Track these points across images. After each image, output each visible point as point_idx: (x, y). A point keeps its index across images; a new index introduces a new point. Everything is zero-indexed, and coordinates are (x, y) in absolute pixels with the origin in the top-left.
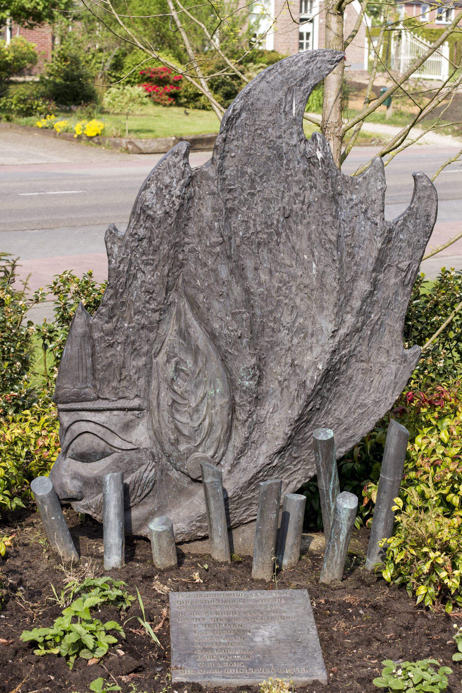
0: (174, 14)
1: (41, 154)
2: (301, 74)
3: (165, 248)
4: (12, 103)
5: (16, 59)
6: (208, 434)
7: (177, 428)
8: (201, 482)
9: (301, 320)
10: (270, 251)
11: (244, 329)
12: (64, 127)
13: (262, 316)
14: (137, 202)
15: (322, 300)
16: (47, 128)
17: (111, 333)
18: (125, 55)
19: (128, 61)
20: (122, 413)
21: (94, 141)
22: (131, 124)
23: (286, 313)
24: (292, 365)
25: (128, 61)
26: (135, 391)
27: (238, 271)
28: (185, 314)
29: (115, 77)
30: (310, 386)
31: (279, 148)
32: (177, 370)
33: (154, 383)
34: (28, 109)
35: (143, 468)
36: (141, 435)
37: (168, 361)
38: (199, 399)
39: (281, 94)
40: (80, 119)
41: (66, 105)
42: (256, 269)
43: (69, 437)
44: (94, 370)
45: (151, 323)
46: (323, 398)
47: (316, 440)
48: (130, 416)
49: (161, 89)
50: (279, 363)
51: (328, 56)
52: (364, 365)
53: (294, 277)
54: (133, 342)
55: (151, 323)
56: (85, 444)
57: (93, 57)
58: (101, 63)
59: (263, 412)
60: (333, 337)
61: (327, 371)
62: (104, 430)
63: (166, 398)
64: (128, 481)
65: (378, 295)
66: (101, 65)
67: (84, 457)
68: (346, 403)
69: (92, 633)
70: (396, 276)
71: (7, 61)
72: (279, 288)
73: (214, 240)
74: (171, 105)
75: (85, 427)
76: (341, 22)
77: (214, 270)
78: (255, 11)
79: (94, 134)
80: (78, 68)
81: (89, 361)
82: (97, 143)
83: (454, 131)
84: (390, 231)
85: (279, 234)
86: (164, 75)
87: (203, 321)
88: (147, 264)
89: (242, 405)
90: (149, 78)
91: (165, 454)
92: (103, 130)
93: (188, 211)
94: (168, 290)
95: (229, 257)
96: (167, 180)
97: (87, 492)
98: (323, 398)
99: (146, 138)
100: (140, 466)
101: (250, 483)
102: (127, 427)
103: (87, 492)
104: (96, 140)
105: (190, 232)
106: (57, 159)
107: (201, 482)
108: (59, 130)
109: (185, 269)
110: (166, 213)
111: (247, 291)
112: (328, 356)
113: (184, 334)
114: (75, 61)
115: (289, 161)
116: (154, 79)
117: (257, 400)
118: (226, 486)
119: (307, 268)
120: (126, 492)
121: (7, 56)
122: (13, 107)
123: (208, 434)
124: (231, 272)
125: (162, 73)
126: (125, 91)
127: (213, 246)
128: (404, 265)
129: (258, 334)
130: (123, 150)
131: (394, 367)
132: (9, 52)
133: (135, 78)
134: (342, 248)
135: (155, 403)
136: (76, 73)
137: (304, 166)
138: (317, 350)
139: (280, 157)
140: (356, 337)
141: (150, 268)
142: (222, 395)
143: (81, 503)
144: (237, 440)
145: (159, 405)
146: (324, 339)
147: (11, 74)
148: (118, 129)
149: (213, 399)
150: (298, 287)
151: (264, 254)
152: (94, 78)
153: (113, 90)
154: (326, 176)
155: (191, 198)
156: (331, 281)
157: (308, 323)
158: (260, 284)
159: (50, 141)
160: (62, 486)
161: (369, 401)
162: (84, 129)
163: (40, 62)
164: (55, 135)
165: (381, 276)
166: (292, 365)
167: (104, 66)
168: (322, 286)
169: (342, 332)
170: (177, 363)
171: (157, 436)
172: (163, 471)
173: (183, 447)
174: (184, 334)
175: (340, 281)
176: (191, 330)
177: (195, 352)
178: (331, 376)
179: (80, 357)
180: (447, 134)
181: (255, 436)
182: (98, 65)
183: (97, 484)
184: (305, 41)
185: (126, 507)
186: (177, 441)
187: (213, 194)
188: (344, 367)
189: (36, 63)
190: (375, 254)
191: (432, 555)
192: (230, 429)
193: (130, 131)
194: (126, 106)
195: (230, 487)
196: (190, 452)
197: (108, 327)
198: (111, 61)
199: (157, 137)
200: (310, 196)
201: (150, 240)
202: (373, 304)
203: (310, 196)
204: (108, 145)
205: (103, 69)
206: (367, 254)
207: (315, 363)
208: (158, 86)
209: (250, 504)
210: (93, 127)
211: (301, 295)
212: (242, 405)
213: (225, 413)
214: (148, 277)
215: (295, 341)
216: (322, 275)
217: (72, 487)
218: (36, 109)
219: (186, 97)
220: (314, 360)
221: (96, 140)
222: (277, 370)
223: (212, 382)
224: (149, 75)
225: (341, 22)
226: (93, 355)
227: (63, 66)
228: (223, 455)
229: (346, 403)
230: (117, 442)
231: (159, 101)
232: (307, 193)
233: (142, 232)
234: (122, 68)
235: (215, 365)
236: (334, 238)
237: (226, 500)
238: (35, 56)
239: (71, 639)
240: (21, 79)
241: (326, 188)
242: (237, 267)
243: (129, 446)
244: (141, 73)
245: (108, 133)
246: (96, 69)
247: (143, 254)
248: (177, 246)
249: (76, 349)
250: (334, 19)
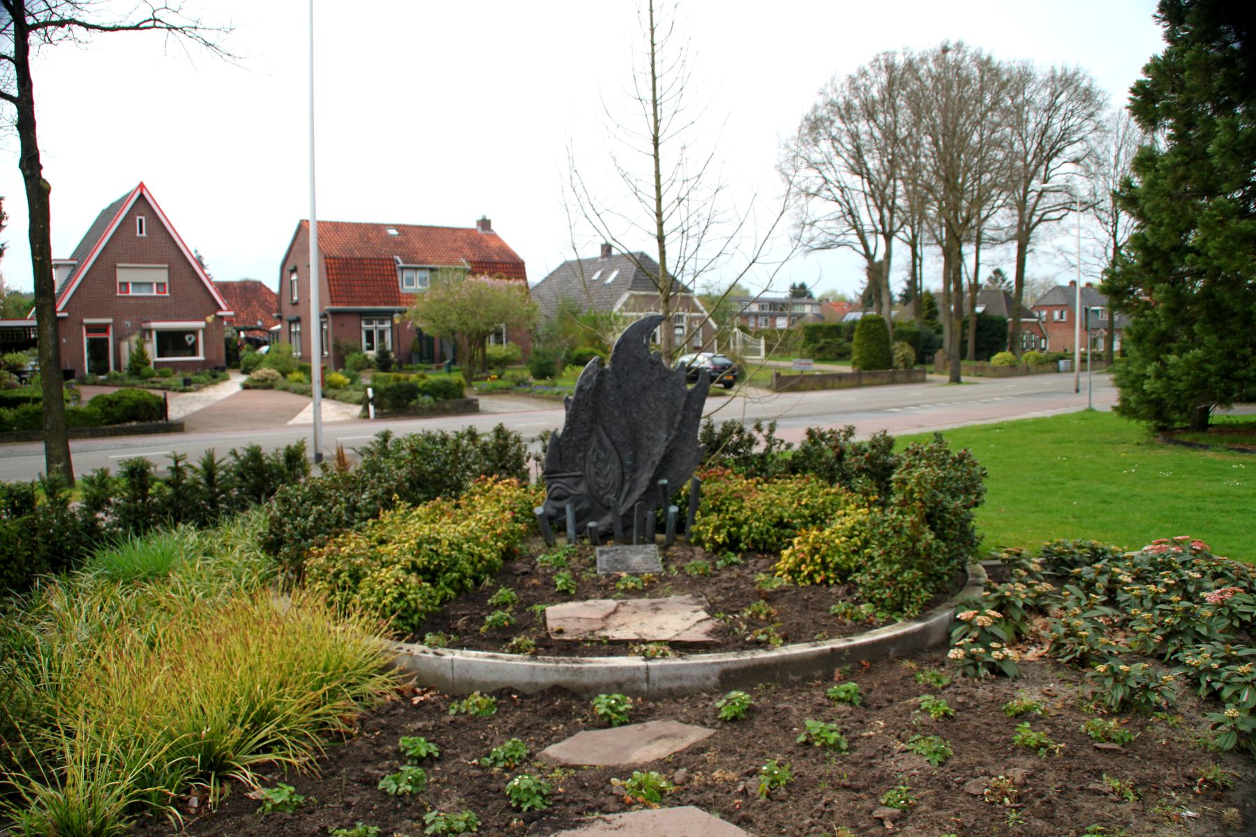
28: (248, 714)
36: (582, 488)
63: (593, 470)
87: (608, 436)
89: (628, 472)
102: (576, 484)
113: (600, 441)
117: (635, 470)
171: (589, 488)
174: (600, 441)
177: (605, 450)
220: (659, 450)
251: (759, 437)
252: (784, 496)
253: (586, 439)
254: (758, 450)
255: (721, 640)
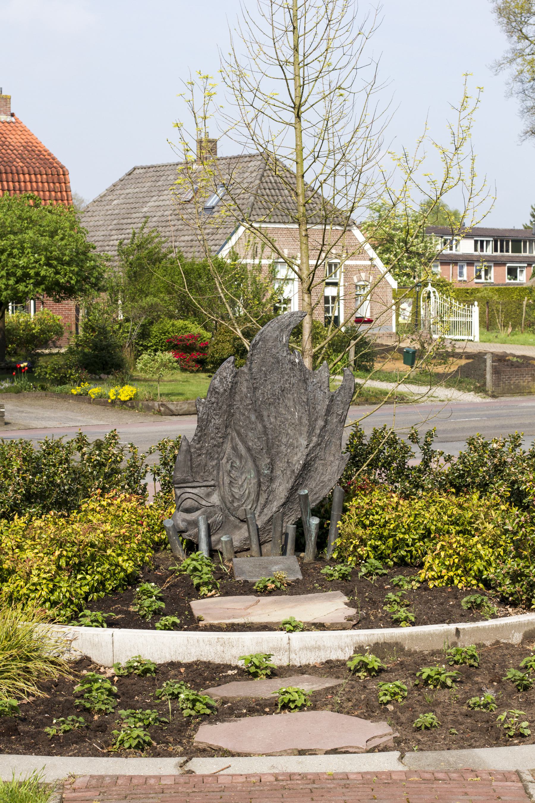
0: (222, 295)
1: (79, 418)
2: (287, 323)
3: (224, 407)
4: (46, 373)
5: (42, 331)
6: (248, 498)
7: (232, 495)
8: (245, 521)
9: (291, 440)
10: (275, 407)
11: (264, 445)
12: (98, 393)
13: (272, 439)
14: (210, 385)
15: (301, 430)
16: (81, 395)
17: (200, 449)
18: (151, 323)
19: (155, 329)
20: (205, 488)
21: (128, 406)
22: (161, 389)
23: (284, 437)
24: (288, 462)
25: (155, 329)
26: (212, 477)
27: (260, 417)
29: (142, 345)
30: (297, 472)
31: (278, 358)
32: (232, 466)
33: (221, 473)
34: (62, 377)
35: (217, 515)
36: (215, 499)
37: (227, 462)
38: (243, 480)
39: (277, 332)
40: (113, 386)
41: (96, 374)
42: (269, 416)
43: (180, 501)
44: (192, 467)
45: (219, 443)
46: (303, 478)
47: (299, 495)
48: (210, 489)
49: (188, 356)
50: (281, 462)
51: (299, 314)
52: (323, 462)
53: (287, 420)
54: (210, 453)
55: (219, 443)
56: (188, 504)
57: (120, 328)
58: (128, 332)
59: (274, 486)
60: (307, 448)
61: (305, 465)
62: (197, 497)
63: (227, 480)
64: (209, 522)
65: (328, 427)
66: (129, 334)
67: (188, 511)
68: (315, 481)
69: (200, 564)
70: (336, 418)
71: (34, 334)
72: (280, 425)
73: (248, 402)
74: (198, 371)
75: (188, 495)
76: (310, 297)
77: (248, 417)
78: (279, 276)
79: (127, 398)
80: (105, 338)
81: (189, 463)
82: (130, 407)
83: (476, 387)
84: (333, 396)
85: (279, 399)
86: (190, 342)
88: (216, 415)
89: (264, 483)
90: (176, 345)
91: (227, 508)
92: (136, 395)
93: (235, 389)
94: (226, 427)
95: (255, 410)
96: (225, 374)
97: (190, 528)
98: (303, 478)
99: (177, 400)
100: (215, 514)
101: (269, 521)
102: (209, 495)
103: (190, 528)
104: (130, 405)
105: (236, 399)
106: (95, 422)
107: (245, 521)
108: (93, 396)
109: (234, 417)
110: (225, 390)
111: (264, 427)
112: (305, 457)
113: (235, 448)
114: (103, 331)
115: (283, 364)
116: (180, 346)
117: (271, 480)
118: (257, 523)
119: (293, 414)
120: (209, 528)
121: (34, 329)
122: (48, 376)
123: (248, 498)
124: (257, 418)
125: (188, 340)
126: (156, 357)
127: (248, 405)
128: (340, 412)
129: (271, 448)
130: (156, 412)
131: (337, 462)
132: (35, 325)
133: (162, 346)
134: (310, 405)
135: (221, 483)
136: (104, 343)
137: (290, 366)
138: (300, 454)
139: (278, 362)
140: (318, 448)
141: (217, 417)
142: (254, 478)
143: (187, 534)
144: (262, 500)
145: (223, 483)
146: (302, 449)
147: (37, 347)
148: (150, 393)
149: (250, 480)
150: (289, 425)
151: (272, 409)
152: (122, 346)
153: (145, 356)
154: (301, 371)
155: (236, 383)
156: (305, 421)
157: (295, 442)
158: (271, 424)
159: (85, 406)
160: (178, 525)
161: (326, 480)
162: (117, 394)
163: (66, 334)
164: (90, 401)
165: (329, 418)
166: (288, 462)
167: (131, 335)
168: (301, 423)
169: (311, 445)
170: (232, 463)
171: (223, 499)
172: (226, 517)
173: (235, 504)
174: (235, 448)
175: (309, 421)
176: (238, 447)
177: (240, 457)
178: (307, 467)
179: (185, 461)
180: (469, 391)
181: (271, 498)
182: (125, 335)
183: (195, 524)
184: (331, 305)
185: (209, 536)
186: (233, 501)
187: (247, 380)
188: (313, 463)
189: (62, 334)
190: (325, 407)
191: (354, 542)
192: (258, 495)
193: (161, 395)
194: (157, 371)
195: (259, 524)
196: (239, 507)
197: (197, 446)
198: (137, 330)
199: (187, 399)
200: (293, 380)
201: (217, 403)
202: (326, 431)
203: (293, 380)
204: (141, 408)
205: (130, 339)
206: (322, 408)
207: (299, 461)
208: (185, 353)
209: (270, 532)
210: (126, 392)
211: (291, 428)
212: (264, 483)
213: (256, 487)
214: (217, 421)
215: (289, 450)
216: (300, 418)
217: (182, 525)
218: (69, 377)
219: (212, 363)
220: (298, 460)
221: (130, 405)
222: (280, 465)
223: (249, 472)
224: (176, 342)
225: (310, 297)
226: (191, 460)
227: (91, 336)
228: (256, 508)
229: (315, 481)
230: (204, 503)
231: (186, 367)
232: (292, 379)
233: (213, 400)
234: (149, 336)
235: (250, 464)
236: (305, 400)
237: (258, 529)
238: (61, 328)
239: (191, 568)
240: (47, 351)
241: (300, 376)
242: (260, 415)
243: (210, 505)
244: (167, 341)
245: (141, 397)
246: (125, 338)
247: (214, 410)
248: (230, 406)
249: (183, 457)
250: (306, 296)
251: (415, 449)
252: (432, 509)
253: (220, 445)
254: (415, 462)
255: (361, 623)
